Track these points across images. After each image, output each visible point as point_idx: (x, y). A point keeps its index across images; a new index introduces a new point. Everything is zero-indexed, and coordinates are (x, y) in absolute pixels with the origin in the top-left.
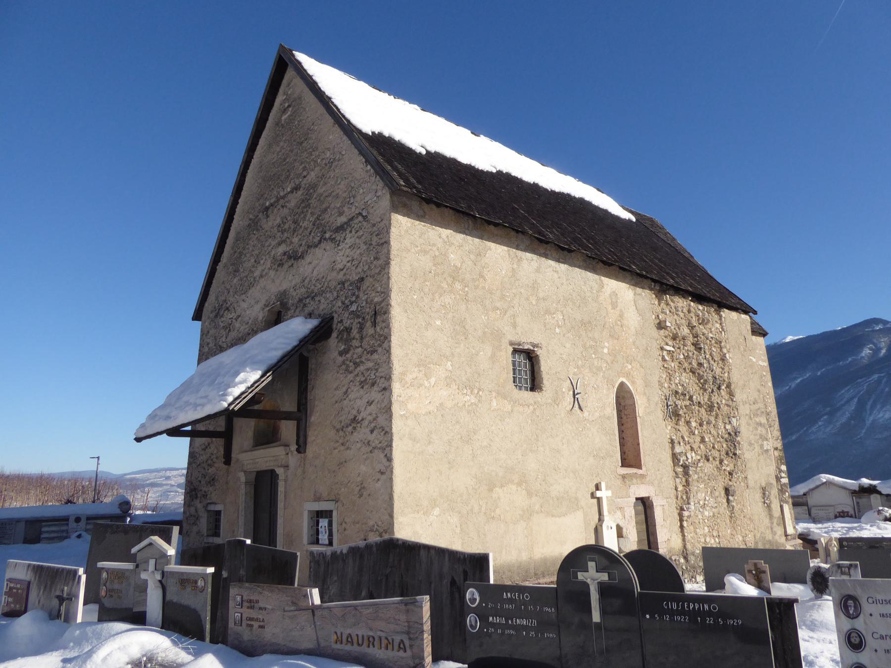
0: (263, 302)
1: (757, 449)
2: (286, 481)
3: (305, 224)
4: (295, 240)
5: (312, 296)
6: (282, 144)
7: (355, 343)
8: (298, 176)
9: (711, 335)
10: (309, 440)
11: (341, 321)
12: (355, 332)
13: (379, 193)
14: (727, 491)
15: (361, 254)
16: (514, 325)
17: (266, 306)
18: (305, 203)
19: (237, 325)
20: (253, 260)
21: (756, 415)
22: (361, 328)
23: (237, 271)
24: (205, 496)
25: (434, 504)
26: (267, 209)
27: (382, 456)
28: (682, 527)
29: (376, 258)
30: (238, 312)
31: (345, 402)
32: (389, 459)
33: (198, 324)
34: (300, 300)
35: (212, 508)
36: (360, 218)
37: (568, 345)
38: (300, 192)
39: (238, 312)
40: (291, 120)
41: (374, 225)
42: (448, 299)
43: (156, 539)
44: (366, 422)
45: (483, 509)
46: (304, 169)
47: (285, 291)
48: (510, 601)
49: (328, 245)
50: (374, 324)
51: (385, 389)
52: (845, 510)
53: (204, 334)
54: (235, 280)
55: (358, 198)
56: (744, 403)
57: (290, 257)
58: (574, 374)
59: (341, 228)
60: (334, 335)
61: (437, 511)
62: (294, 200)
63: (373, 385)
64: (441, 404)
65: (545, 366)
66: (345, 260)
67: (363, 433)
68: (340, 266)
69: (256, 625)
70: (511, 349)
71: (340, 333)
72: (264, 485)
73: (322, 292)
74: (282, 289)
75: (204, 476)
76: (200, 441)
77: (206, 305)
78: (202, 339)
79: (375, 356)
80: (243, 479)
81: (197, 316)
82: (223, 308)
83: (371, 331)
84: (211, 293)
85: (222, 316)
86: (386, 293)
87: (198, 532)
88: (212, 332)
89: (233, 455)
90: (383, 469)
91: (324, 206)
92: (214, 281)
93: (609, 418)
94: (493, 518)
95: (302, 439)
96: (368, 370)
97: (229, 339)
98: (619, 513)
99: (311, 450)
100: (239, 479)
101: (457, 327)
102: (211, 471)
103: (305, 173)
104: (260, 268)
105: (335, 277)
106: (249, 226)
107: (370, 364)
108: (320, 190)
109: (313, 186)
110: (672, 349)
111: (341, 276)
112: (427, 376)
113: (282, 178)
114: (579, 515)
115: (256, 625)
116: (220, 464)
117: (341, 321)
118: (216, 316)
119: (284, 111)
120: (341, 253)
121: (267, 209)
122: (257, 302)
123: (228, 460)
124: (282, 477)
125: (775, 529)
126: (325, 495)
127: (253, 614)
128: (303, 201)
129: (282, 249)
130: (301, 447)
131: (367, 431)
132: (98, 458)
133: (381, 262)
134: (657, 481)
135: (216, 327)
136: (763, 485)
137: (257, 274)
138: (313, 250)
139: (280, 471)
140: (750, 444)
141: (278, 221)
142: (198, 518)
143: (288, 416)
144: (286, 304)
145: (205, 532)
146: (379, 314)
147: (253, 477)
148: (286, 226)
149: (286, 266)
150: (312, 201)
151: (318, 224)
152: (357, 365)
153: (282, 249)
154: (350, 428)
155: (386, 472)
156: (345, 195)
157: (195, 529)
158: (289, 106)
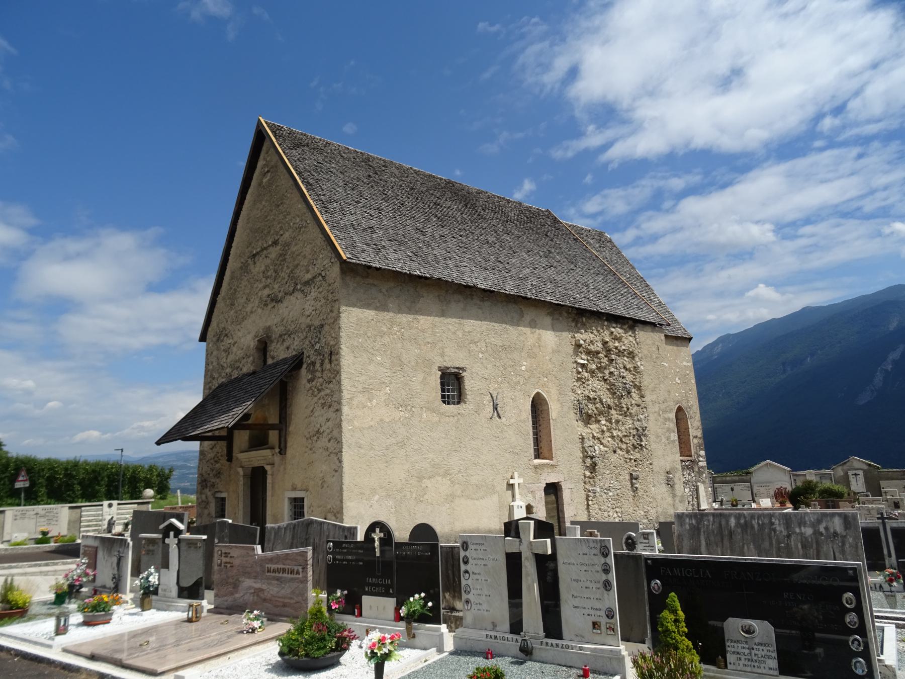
0: (253, 334)
1: (664, 440)
2: (272, 475)
3: (283, 274)
4: (276, 286)
5: (289, 334)
6: (264, 203)
7: (318, 374)
8: (277, 233)
9: (623, 347)
10: (289, 444)
11: (309, 357)
12: (318, 366)
13: (333, 260)
14: (632, 477)
15: (321, 306)
16: (442, 355)
17: (256, 336)
18: (282, 256)
19: (234, 349)
20: (245, 298)
21: (665, 411)
22: (322, 364)
23: (233, 304)
24: (213, 486)
25: (374, 491)
26: (254, 256)
27: (336, 458)
28: (588, 505)
29: (331, 311)
30: (236, 339)
31: (312, 418)
32: (340, 461)
33: (204, 344)
34: (281, 336)
35: (219, 495)
36: (320, 278)
37: (489, 366)
38: (279, 247)
39: (236, 339)
40: (270, 183)
41: (330, 285)
42: (386, 340)
43: (174, 521)
44: (325, 434)
45: (414, 495)
46: (281, 228)
47: (269, 327)
48: (345, 548)
49: (299, 295)
50: (330, 361)
51: (337, 410)
52: (784, 486)
53: (209, 354)
54: (232, 312)
55: (319, 261)
56: (654, 402)
57: (272, 300)
58: (495, 389)
59: (307, 283)
60: (304, 366)
61: (377, 497)
62: (274, 252)
63: (330, 407)
64: (381, 420)
65: (469, 384)
66: (311, 309)
67: (323, 442)
68: (307, 313)
69: (229, 565)
70: (440, 373)
71: (308, 365)
72: (257, 480)
73: (295, 332)
74: (268, 324)
75: (212, 470)
76: (206, 443)
77: (210, 329)
78: (207, 358)
79: (331, 386)
80: (241, 473)
81: (203, 338)
82: (223, 334)
83: (328, 366)
84: (213, 320)
85: (222, 341)
86: (337, 338)
87: (209, 514)
88: (215, 353)
89: (234, 454)
90: (336, 468)
91: (296, 263)
92: (215, 310)
93: (524, 422)
94: (422, 501)
95: (282, 445)
96: (326, 395)
97: (228, 360)
98: (530, 495)
99: (290, 452)
100: (238, 473)
101: (395, 361)
102: (218, 466)
103: (281, 232)
104: (251, 305)
105: (304, 321)
106: (241, 268)
107: (328, 391)
108: (294, 249)
109: (287, 245)
110: (585, 362)
111: (308, 320)
112: (370, 400)
113: (265, 232)
114: (495, 498)
115: (229, 565)
116: (224, 461)
117: (309, 357)
118: (218, 340)
119: (265, 174)
120: (308, 303)
121: (254, 256)
122: (249, 333)
123: (230, 458)
124: (269, 472)
125: (676, 506)
126: (299, 486)
127: (228, 560)
128: (281, 255)
129: (267, 292)
130: (283, 451)
131: (326, 440)
132: (122, 450)
133: (334, 315)
134: (566, 468)
135: (218, 349)
136: (668, 470)
137: (248, 309)
138: (288, 297)
139: (268, 468)
140: (658, 437)
141: (263, 268)
142: (208, 503)
143: (273, 427)
144: (271, 337)
145: (213, 514)
146: (332, 354)
147: (249, 471)
148: (269, 274)
149: (270, 307)
150: (287, 257)
151: (292, 276)
152: (319, 391)
153: (267, 292)
154: (315, 438)
155: (338, 470)
156: (310, 257)
157: (206, 512)
158: (268, 171)
